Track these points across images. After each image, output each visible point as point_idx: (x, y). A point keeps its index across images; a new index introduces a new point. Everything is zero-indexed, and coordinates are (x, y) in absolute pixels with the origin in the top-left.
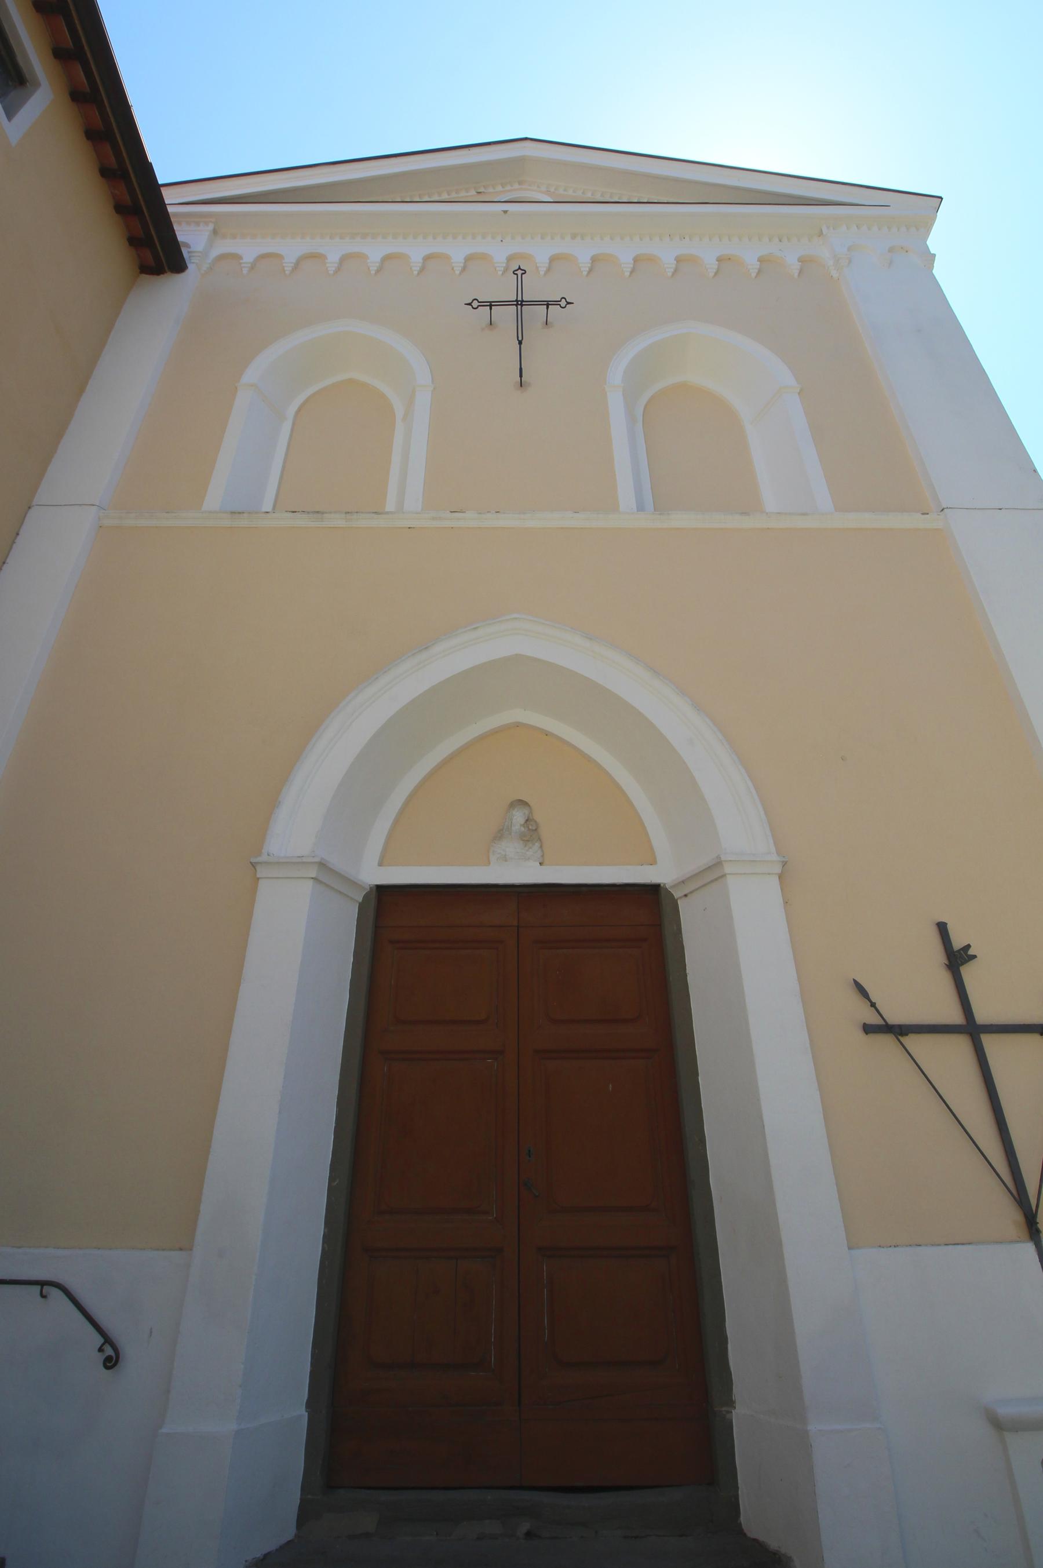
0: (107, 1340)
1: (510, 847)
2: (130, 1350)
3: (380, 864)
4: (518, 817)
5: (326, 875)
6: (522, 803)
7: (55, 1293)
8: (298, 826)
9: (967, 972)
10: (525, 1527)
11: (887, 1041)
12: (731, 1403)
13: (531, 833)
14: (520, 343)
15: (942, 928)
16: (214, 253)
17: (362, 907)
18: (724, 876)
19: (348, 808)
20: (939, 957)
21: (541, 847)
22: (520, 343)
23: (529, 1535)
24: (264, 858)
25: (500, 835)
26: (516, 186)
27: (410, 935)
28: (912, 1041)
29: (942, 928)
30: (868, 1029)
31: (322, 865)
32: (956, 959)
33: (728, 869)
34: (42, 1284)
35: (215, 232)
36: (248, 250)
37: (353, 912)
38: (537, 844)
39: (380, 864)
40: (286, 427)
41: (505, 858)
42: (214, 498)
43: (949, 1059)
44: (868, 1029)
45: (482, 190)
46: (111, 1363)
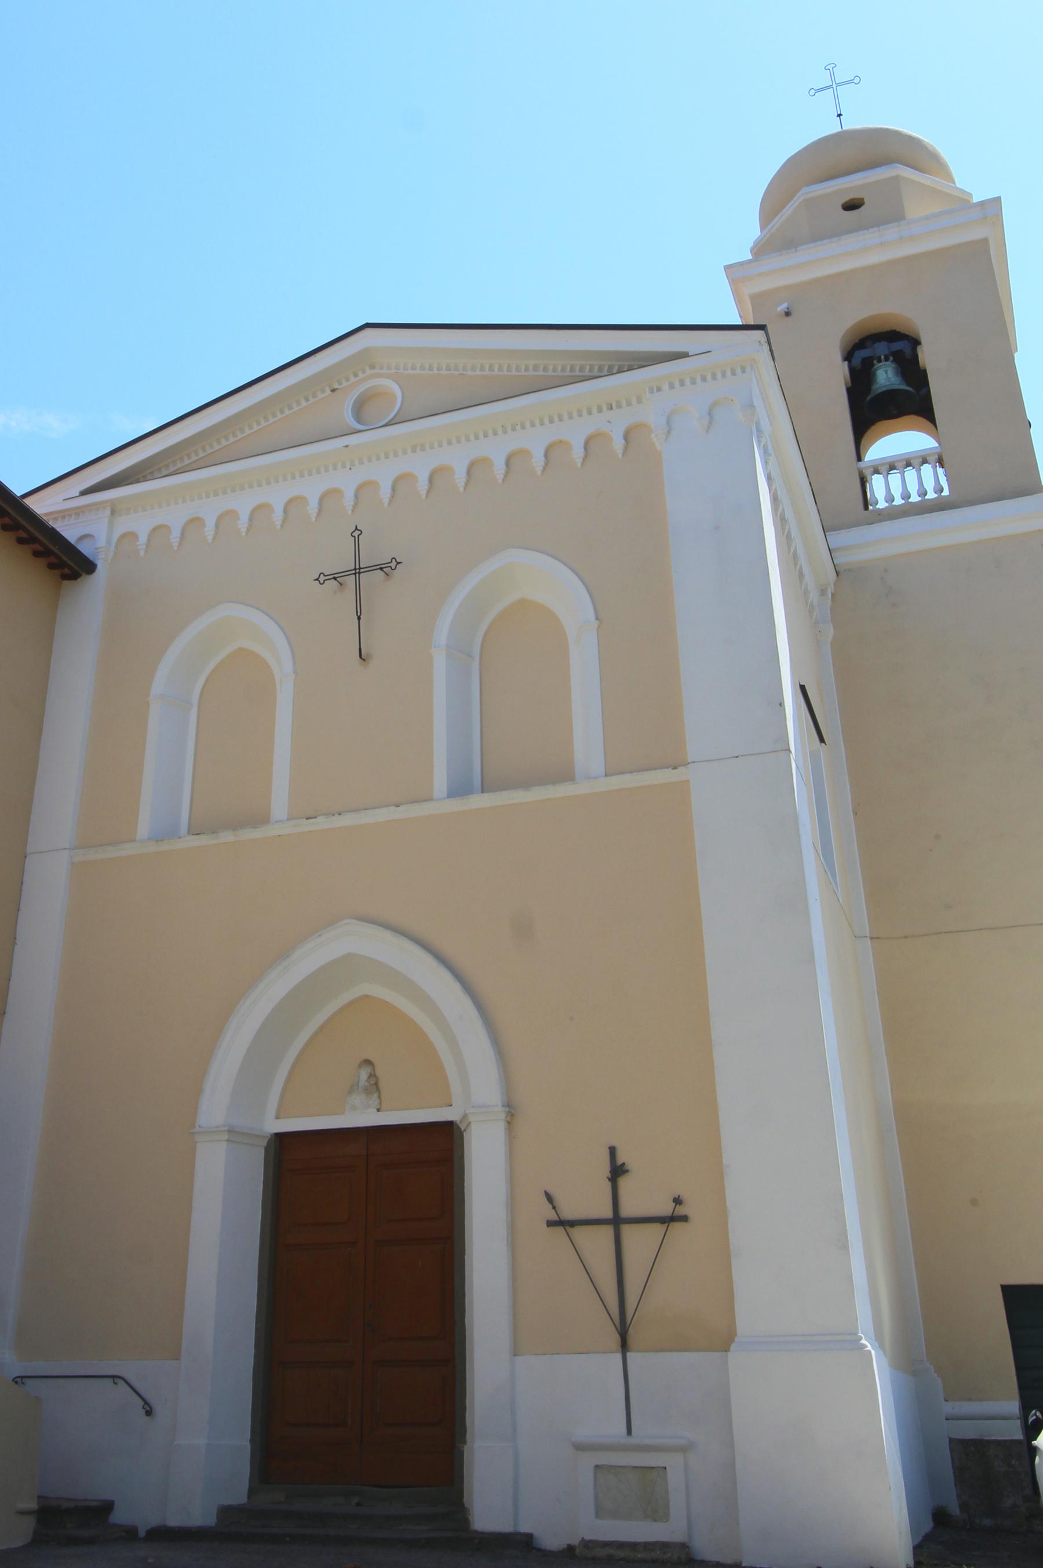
0: (146, 1402)
1: (357, 1099)
2: (158, 1408)
3: (277, 1117)
4: (364, 1074)
5: (234, 1134)
6: (368, 1062)
7: (121, 1382)
8: (215, 1107)
9: (623, 1183)
10: (356, 1500)
11: (560, 1230)
12: (465, 1442)
13: (374, 1086)
14: (359, 618)
15: (613, 1151)
16: (115, 538)
17: (267, 1149)
18: (470, 1123)
19: (239, 1095)
20: (605, 1170)
21: (379, 1097)
22: (359, 618)
23: (358, 1504)
24: (197, 1129)
25: (351, 1091)
26: (369, 372)
27: (298, 1164)
28: (578, 1232)
29: (613, 1151)
30: (550, 1224)
31: (231, 1131)
32: (617, 1171)
33: (471, 1119)
34: (114, 1377)
35: (113, 512)
36: (141, 524)
37: (261, 1154)
38: (376, 1095)
39: (277, 1117)
40: (194, 711)
41: (354, 1108)
42: (143, 828)
43: (597, 1243)
44: (550, 1224)
45: (336, 386)
46: (149, 1412)
